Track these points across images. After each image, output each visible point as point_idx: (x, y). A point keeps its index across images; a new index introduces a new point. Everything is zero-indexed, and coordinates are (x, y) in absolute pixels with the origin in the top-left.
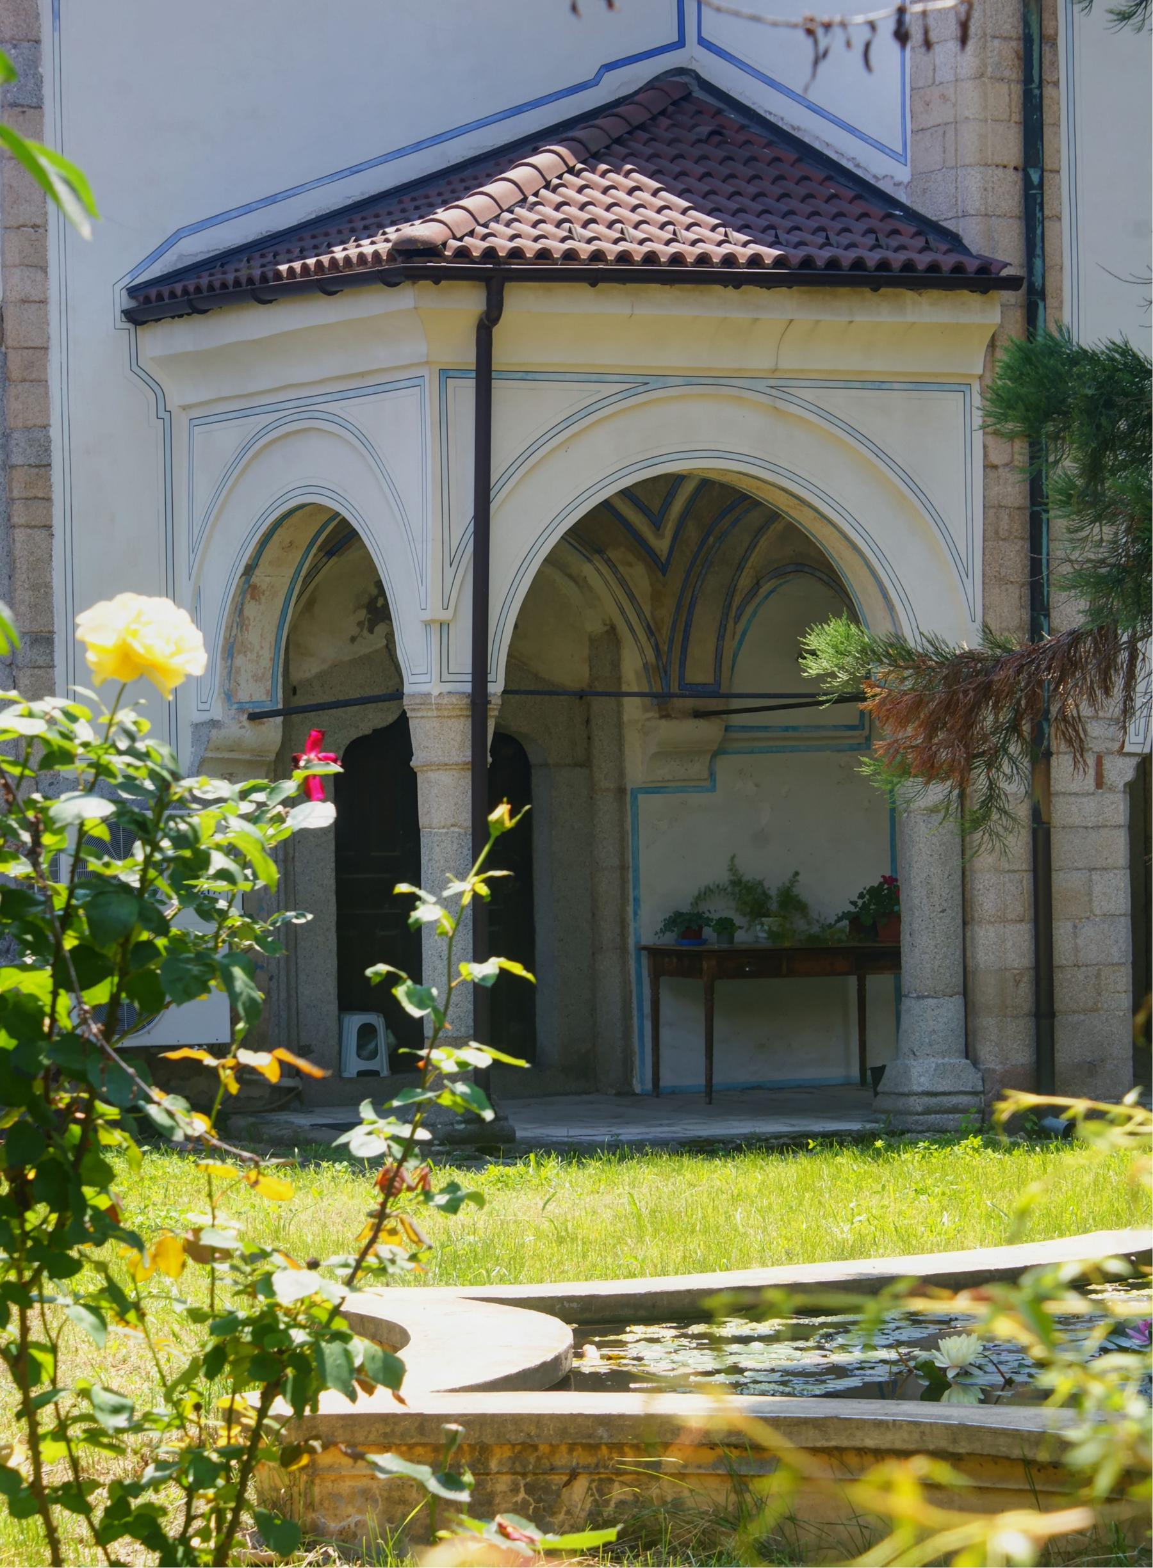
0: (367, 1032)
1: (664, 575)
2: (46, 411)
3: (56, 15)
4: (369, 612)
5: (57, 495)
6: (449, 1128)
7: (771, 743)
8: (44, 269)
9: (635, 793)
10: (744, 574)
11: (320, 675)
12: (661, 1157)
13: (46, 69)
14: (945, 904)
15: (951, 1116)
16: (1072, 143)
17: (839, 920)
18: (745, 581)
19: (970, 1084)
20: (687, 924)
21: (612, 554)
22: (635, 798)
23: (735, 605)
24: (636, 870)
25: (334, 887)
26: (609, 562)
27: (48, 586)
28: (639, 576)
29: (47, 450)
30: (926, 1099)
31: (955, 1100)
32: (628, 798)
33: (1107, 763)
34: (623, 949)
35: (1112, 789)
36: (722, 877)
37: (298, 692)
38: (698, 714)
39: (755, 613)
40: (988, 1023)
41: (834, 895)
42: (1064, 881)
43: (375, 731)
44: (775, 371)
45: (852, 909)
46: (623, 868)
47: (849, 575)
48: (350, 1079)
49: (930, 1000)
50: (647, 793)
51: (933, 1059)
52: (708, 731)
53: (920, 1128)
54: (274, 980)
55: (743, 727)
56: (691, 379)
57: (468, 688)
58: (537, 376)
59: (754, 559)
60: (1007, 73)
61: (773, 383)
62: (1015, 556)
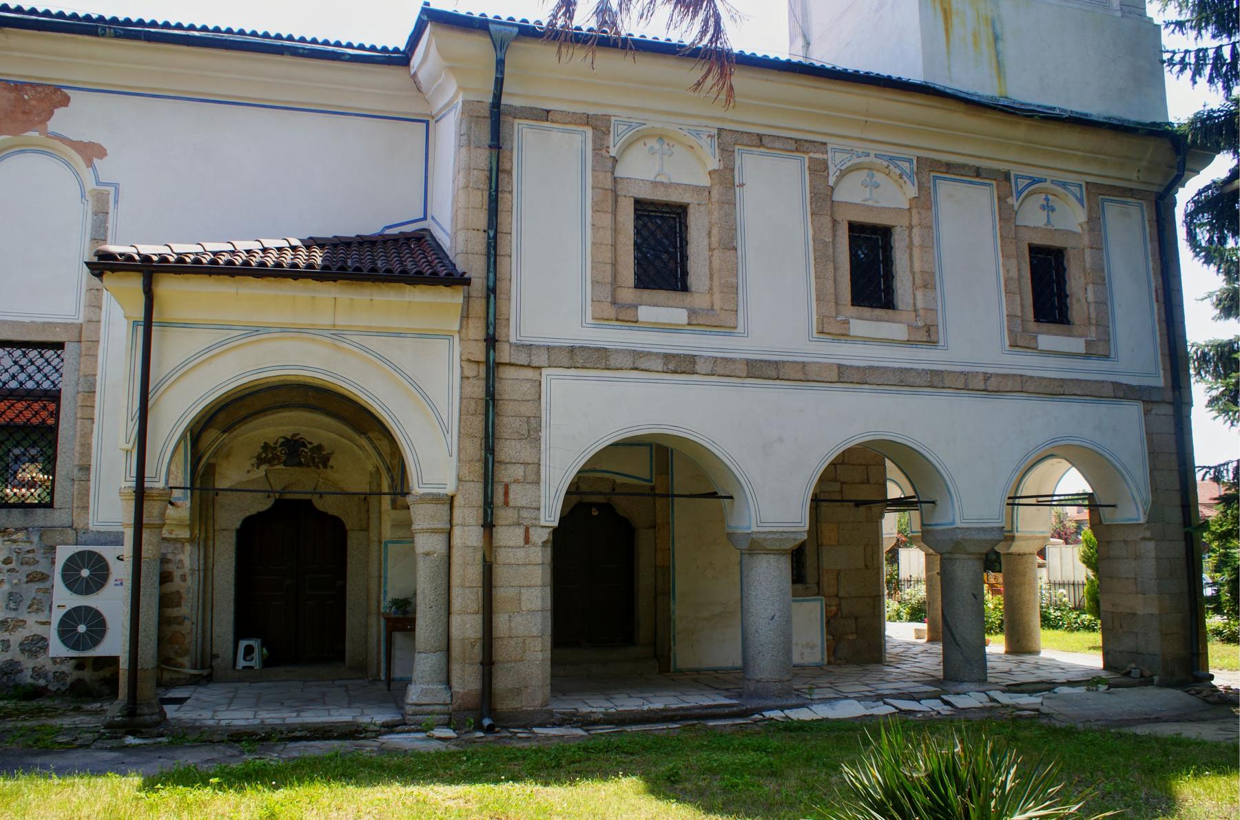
0: (249, 650)
2: (95, 368)
3: (116, 202)
5: (97, 405)
8: (100, 308)
9: (386, 543)
12: (50, 777)
13: (110, 225)
16: (520, 220)
21: (370, 435)
24: (386, 578)
26: (369, 439)
27: (90, 445)
29: (94, 386)
31: (431, 708)
33: (532, 531)
35: (534, 545)
40: (456, 668)
42: (502, 593)
46: (380, 577)
56: (284, 329)
60: (481, 186)
62: (477, 423)
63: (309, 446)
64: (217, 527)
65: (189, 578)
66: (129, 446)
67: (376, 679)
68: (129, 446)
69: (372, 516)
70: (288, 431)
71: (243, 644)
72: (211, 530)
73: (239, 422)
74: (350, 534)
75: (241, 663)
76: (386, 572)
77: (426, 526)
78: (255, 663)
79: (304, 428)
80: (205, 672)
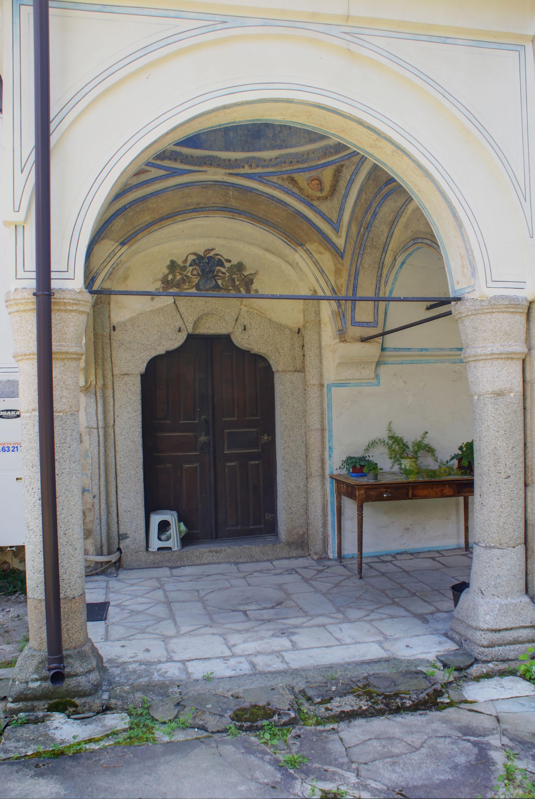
0: (164, 526)
1: (342, 259)
4: (163, 283)
6: (23, 686)
7: (413, 358)
9: (329, 387)
10: (387, 255)
11: (131, 320)
14: (509, 472)
15: (512, 647)
17: (452, 458)
18: (388, 260)
19: (529, 620)
20: (359, 465)
21: (309, 246)
22: (329, 390)
23: (384, 275)
24: (330, 431)
25: (141, 442)
26: (307, 251)
28: (327, 260)
30: (490, 635)
32: (325, 389)
34: (323, 476)
36: (384, 435)
37: (117, 329)
38: (364, 340)
39: (395, 279)
41: (447, 448)
43: (167, 352)
44: (348, 18)
45: (460, 452)
46: (323, 430)
47: (427, 206)
48: (153, 552)
49: (496, 550)
50: (338, 386)
51: (497, 599)
52: (372, 350)
53: (485, 658)
54: (96, 498)
55: (395, 349)
57: (32, 284)
58: (115, 9)
59: (393, 245)
61: (347, 30)
63: (227, 265)
64: (116, 371)
65: (86, 438)
66: (20, 217)
67: (323, 558)
68: (20, 217)
69: (308, 353)
70: (199, 246)
71: (156, 519)
72: (109, 377)
73: (142, 230)
74: (277, 376)
75: (155, 544)
76: (330, 424)
77: (497, 348)
78: (174, 543)
79: (221, 242)
80: (114, 558)
